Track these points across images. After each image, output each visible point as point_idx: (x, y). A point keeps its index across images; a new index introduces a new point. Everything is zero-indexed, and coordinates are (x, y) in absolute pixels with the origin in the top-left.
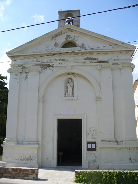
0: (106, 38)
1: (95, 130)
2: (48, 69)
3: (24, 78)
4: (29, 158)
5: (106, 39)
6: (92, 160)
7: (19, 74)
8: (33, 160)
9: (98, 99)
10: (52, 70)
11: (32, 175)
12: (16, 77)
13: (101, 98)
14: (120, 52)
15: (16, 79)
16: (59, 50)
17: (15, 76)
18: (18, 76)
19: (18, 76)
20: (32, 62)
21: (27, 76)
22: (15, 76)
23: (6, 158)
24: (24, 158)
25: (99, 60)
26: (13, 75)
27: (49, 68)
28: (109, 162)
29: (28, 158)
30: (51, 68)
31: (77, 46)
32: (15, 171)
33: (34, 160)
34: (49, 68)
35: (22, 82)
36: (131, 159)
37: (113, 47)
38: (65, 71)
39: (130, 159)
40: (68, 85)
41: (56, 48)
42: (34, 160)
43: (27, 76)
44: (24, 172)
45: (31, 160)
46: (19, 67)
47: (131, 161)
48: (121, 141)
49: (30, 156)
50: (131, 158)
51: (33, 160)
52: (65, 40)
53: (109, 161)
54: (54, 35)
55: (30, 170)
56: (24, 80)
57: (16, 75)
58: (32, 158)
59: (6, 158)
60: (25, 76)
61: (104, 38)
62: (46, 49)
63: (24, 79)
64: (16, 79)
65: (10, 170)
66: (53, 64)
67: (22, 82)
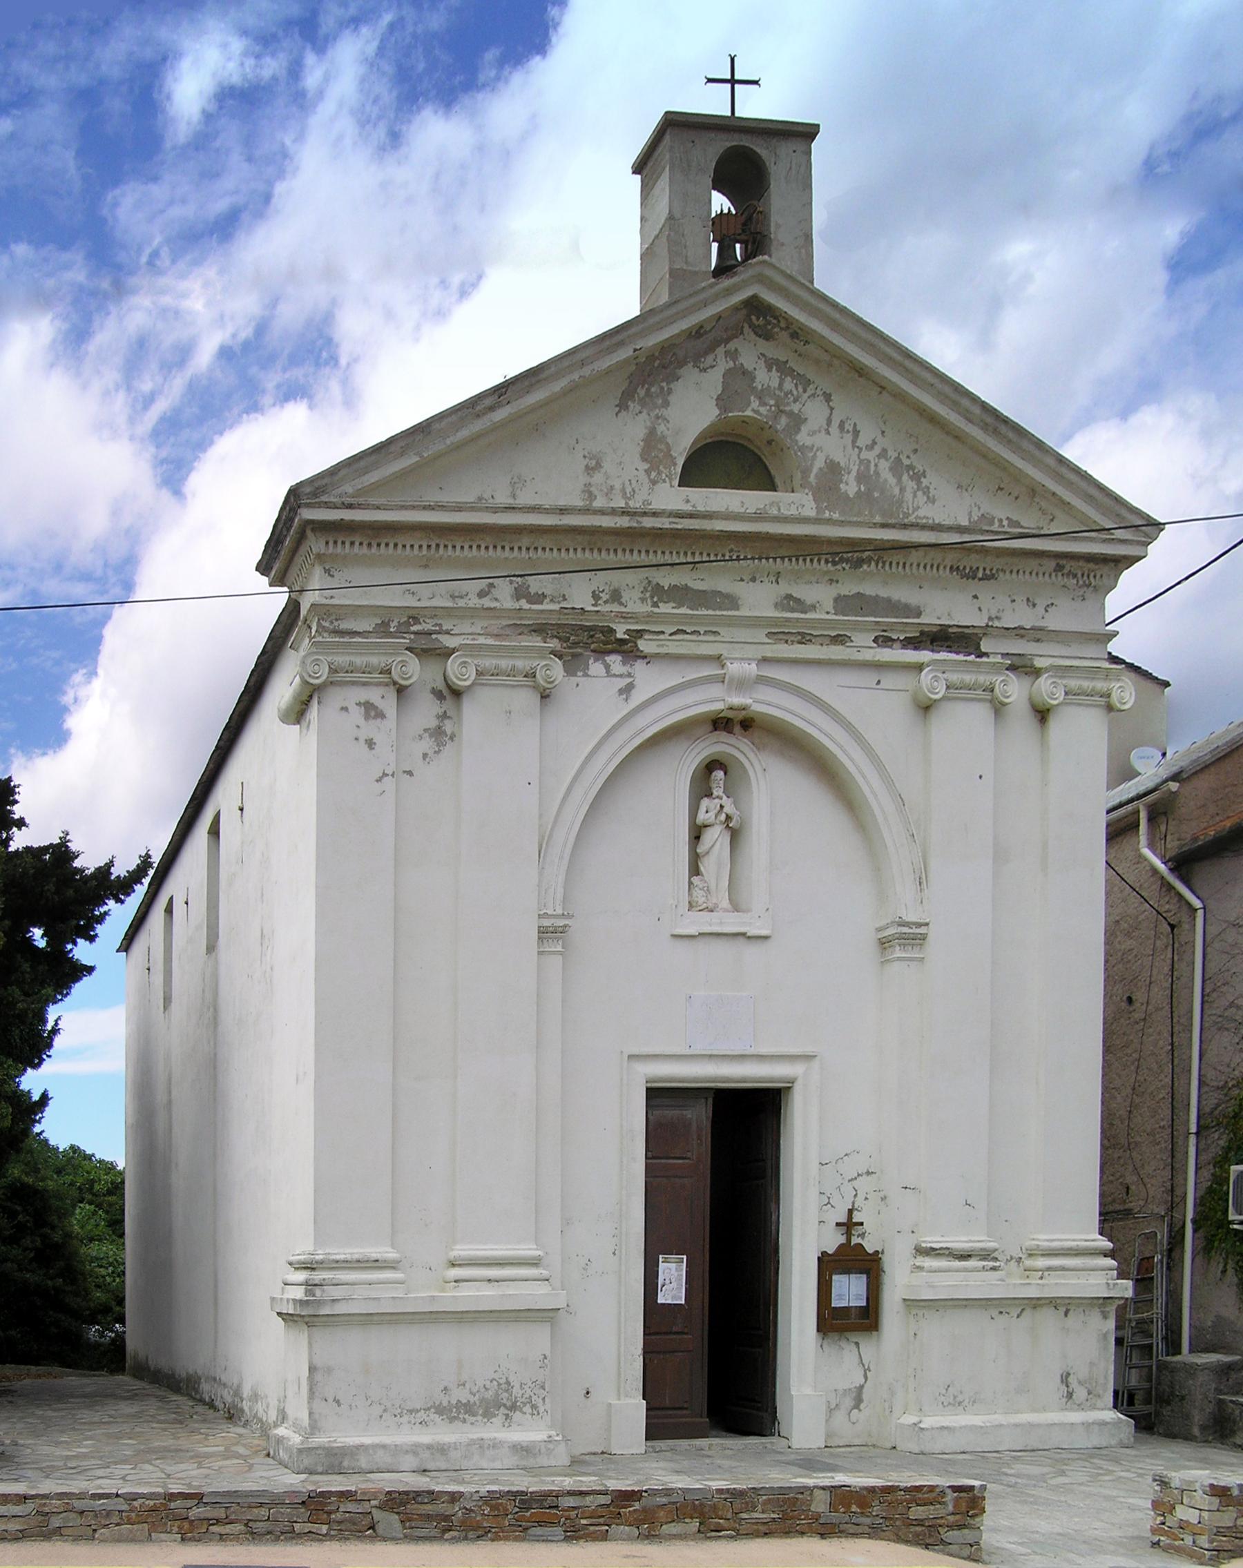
0: (995, 432)
1: (868, 1173)
2: (596, 668)
3: (421, 737)
4: (497, 1394)
5: (992, 444)
6: (846, 1392)
7: (389, 704)
8: (527, 1409)
9: (903, 939)
10: (623, 682)
11: (966, 1531)
12: (370, 729)
13: (922, 930)
14: (1059, 568)
15: (370, 744)
16: (671, 497)
17: (357, 714)
18: (381, 715)
19: (381, 715)
20: (487, 602)
21: (448, 727)
22: (361, 721)
23: (338, 1402)
24: (463, 1396)
25: (930, 619)
26: (345, 709)
27: (607, 667)
28: (960, 1403)
29: (489, 1395)
30: (615, 660)
31: (778, 481)
32: (854, 1508)
33: (534, 1407)
34: (607, 667)
35: (410, 773)
36: (1070, 1379)
37: (848, 588)
38: (714, 700)
39: (1065, 1378)
40: (702, 817)
41: (654, 483)
42: (534, 1407)
43: (448, 727)
44: (917, 1512)
45: (513, 1407)
46: (390, 635)
47: (1070, 1395)
48: (1014, 1255)
49: (508, 1383)
50: (1068, 1374)
51: (521, 1411)
52: (717, 412)
53: (960, 1398)
54: (624, 367)
55: (949, 1491)
56: (425, 756)
57: (372, 712)
58: (516, 1391)
59: (338, 1402)
60: (433, 723)
61: (985, 427)
62: (584, 479)
63: (427, 744)
64: (370, 744)
65: (820, 1504)
66: (640, 634)
67: (410, 773)
